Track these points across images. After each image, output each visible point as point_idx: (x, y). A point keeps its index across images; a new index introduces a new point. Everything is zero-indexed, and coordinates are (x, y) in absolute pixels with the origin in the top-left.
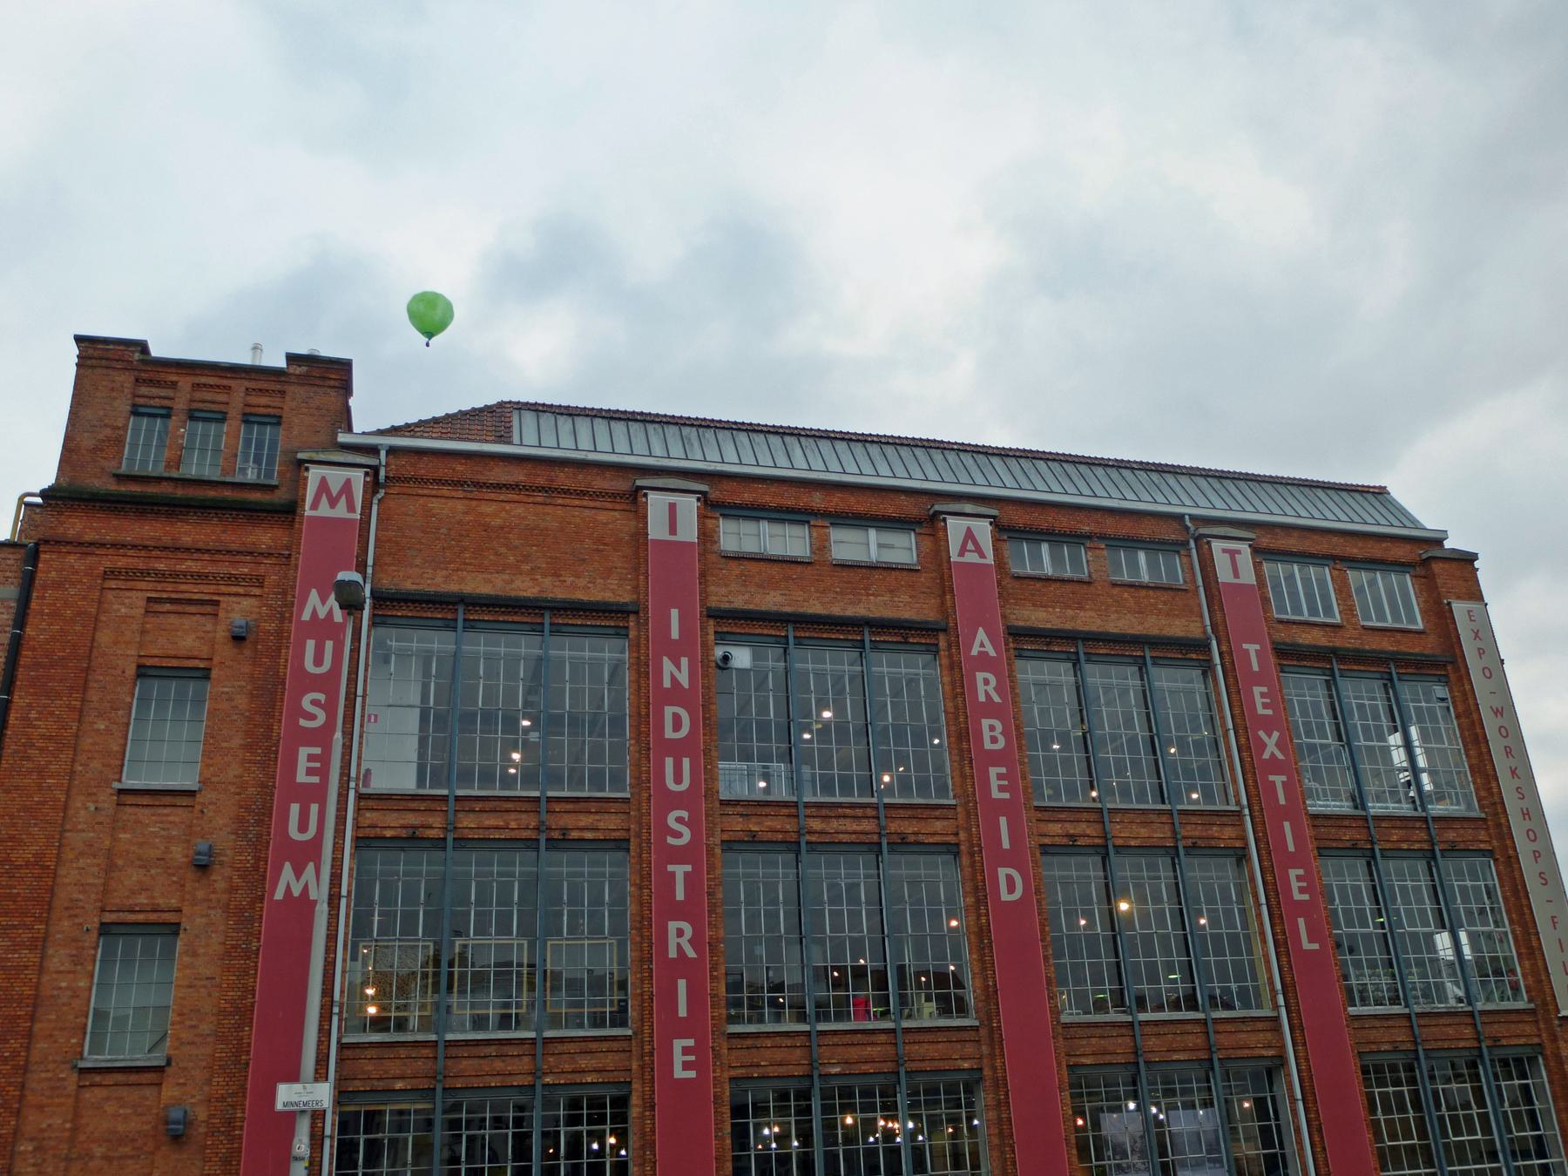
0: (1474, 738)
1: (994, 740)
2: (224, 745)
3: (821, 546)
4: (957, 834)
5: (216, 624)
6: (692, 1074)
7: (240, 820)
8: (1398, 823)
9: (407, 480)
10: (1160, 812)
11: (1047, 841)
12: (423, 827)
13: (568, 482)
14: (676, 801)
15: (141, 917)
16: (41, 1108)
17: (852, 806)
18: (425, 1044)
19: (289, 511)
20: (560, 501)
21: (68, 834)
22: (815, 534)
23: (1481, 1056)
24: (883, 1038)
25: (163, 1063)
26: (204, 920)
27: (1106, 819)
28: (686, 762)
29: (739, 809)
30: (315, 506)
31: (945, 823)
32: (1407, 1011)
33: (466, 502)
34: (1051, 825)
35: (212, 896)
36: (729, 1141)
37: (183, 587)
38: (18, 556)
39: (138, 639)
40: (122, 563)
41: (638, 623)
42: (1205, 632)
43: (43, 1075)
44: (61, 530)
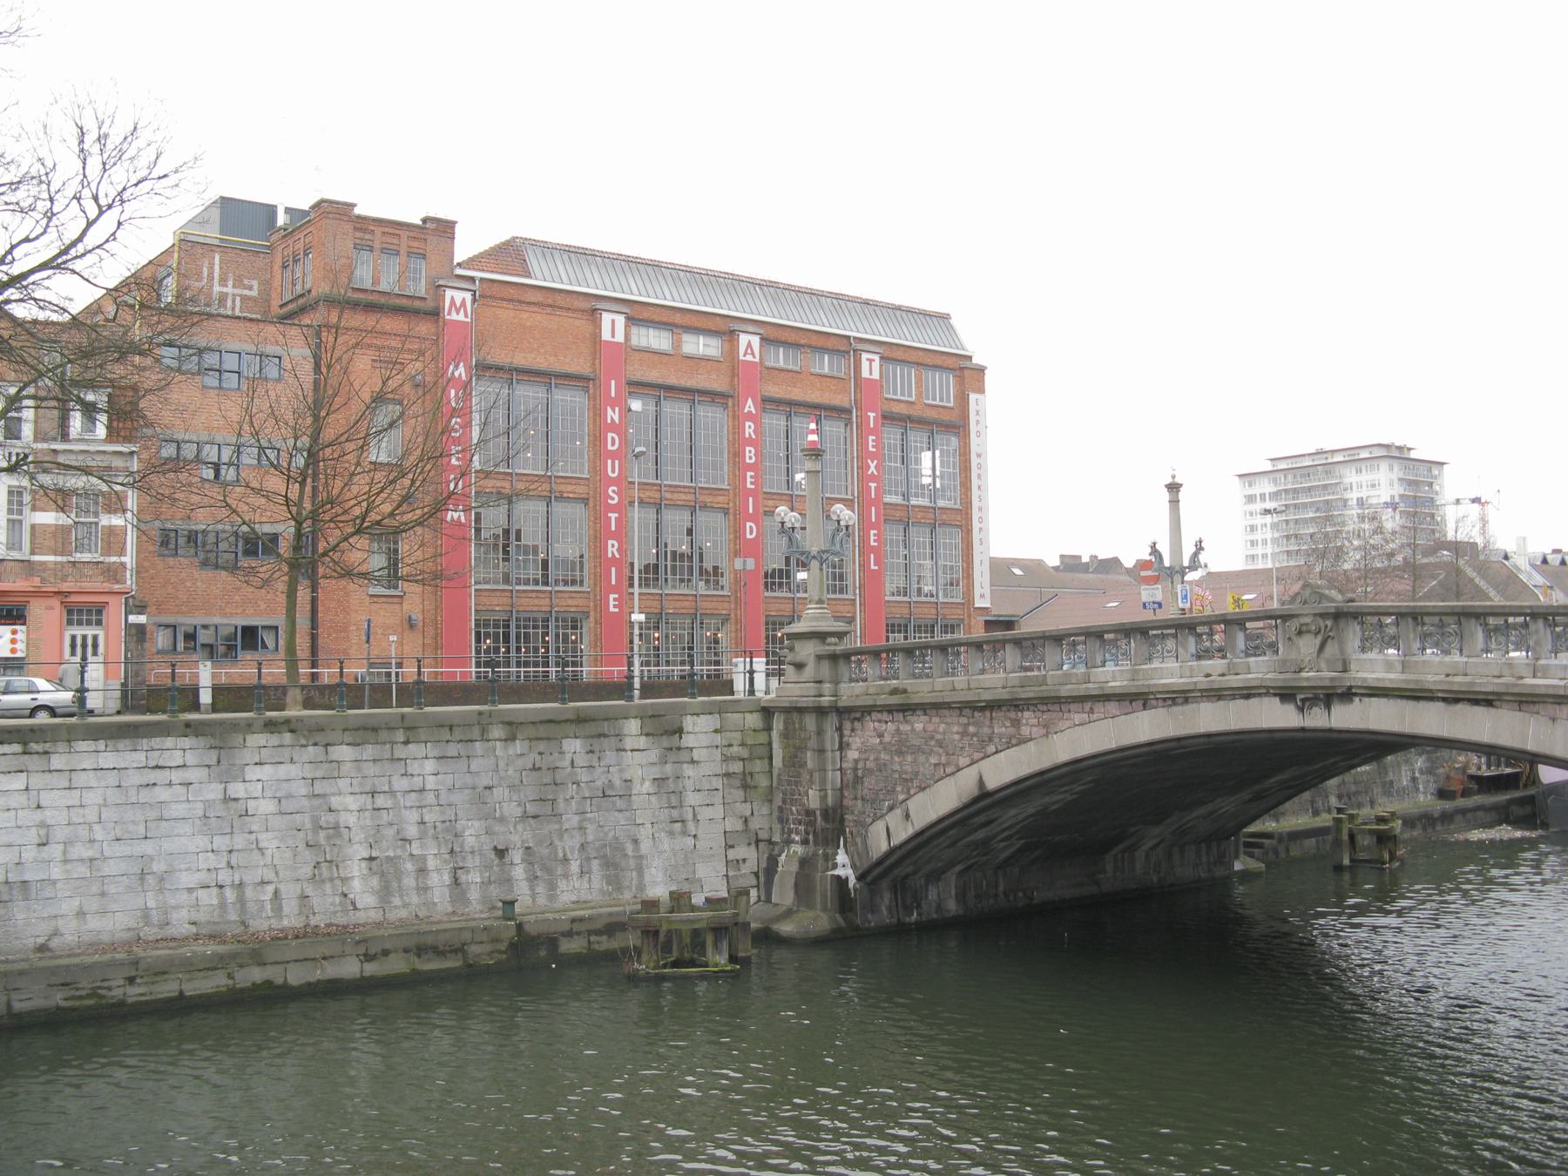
0: (965, 468)
1: (750, 458)
3: (677, 345)
6: (617, 610)
14: (613, 482)
17: (684, 487)
19: (435, 314)
28: (617, 462)
30: (449, 314)
41: (594, 385)
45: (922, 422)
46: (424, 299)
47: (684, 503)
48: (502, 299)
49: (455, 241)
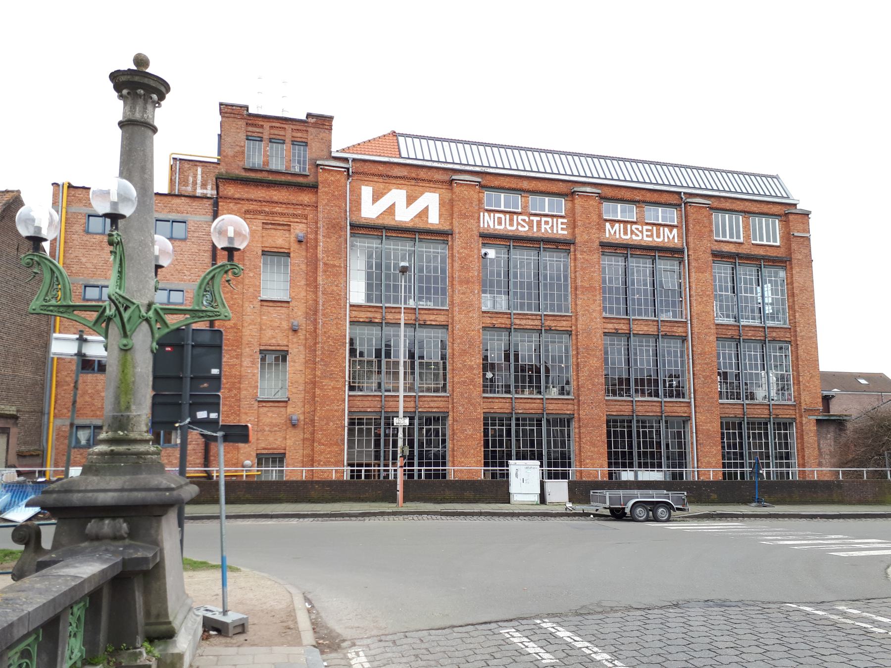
2: (298, 284)
4: (571, 327)
5: (290, 234)
7: (307, 313)
8: (752, 329)
9: (360, 173)
10: (654, 321)
11: (606, 331)
12: (374, 318)
13: (424, 176)
15: (273, 348)
16: (246, 413)
17: (532, 315)
18: (377, 396)
20: (421, 184)
21: (244, 316)
22: (523, 200)
23: (770, 421)
24: (538, 401)
25: (287, 400)
26: (297, 350)
27: (631, 323)
29: (489, 315)
31: (567, 322)
32: (743, 402)
33: (384, 184)
34: (609, 324)
35: (299, 341)
36: (482, 434)
37: (276, 218)
38: (209, 203)
39: (261, 240)
40: (251, 207)
41: (452, 238)
42: (683, 245)
43: (246, 403)
44: (225, 192)
45: (748, 258)
46: (307, 176)
47: (531, 327)
48: (373, 175)
49: (333, 131)
